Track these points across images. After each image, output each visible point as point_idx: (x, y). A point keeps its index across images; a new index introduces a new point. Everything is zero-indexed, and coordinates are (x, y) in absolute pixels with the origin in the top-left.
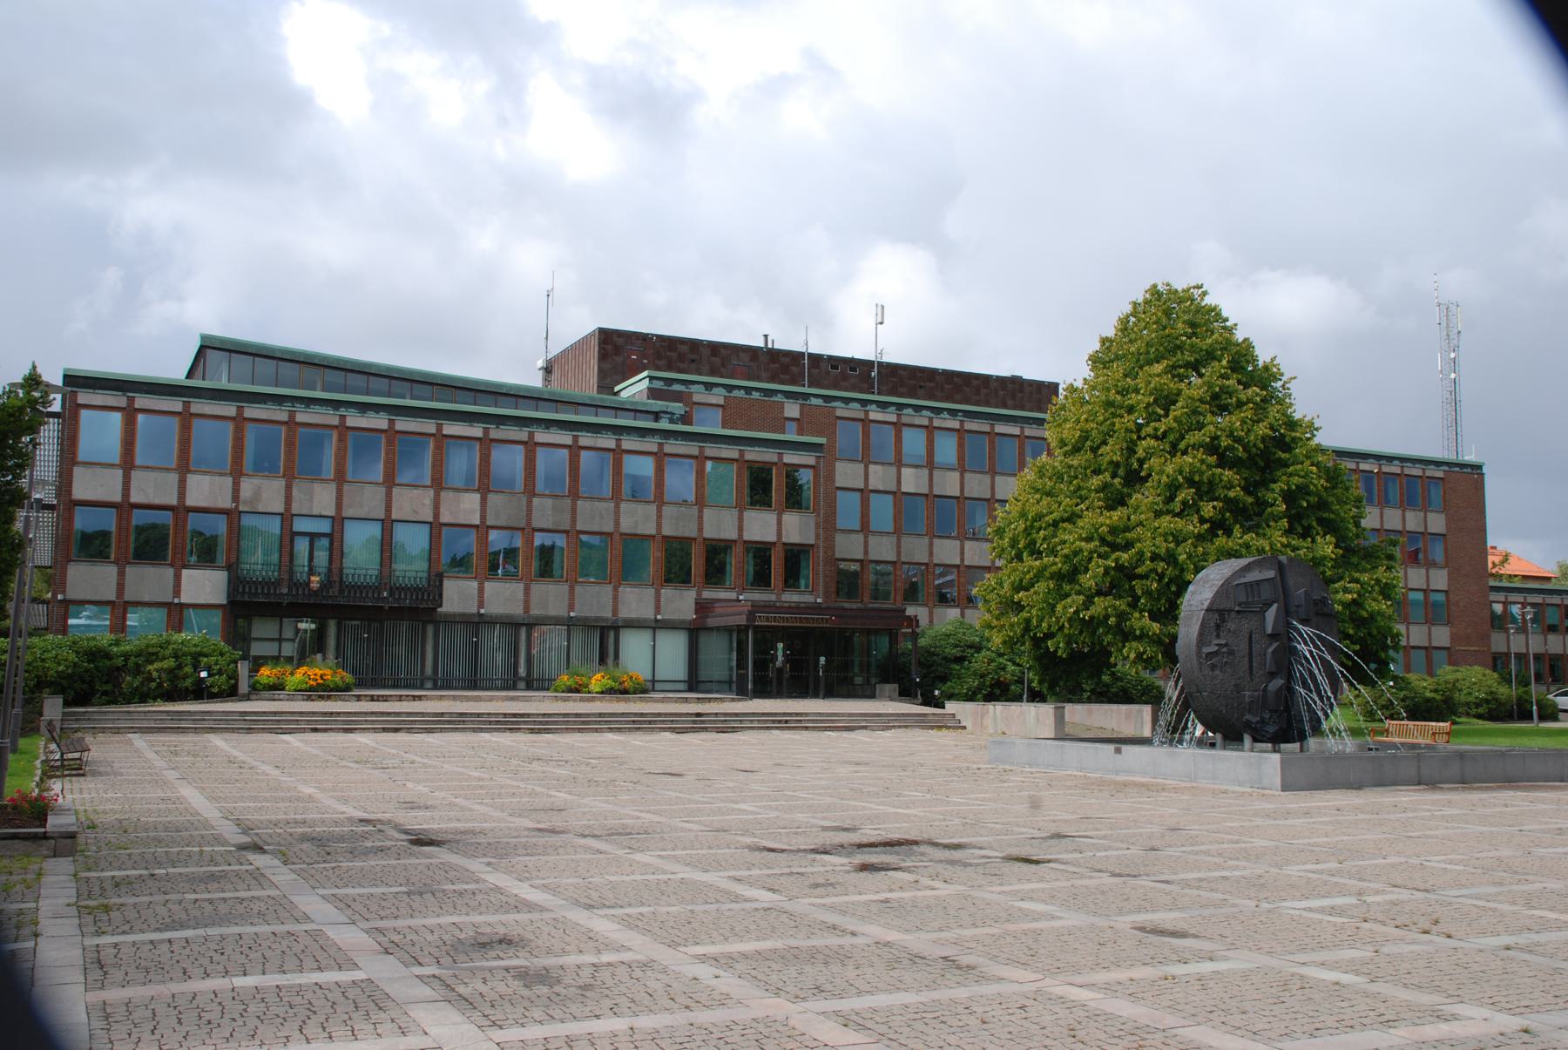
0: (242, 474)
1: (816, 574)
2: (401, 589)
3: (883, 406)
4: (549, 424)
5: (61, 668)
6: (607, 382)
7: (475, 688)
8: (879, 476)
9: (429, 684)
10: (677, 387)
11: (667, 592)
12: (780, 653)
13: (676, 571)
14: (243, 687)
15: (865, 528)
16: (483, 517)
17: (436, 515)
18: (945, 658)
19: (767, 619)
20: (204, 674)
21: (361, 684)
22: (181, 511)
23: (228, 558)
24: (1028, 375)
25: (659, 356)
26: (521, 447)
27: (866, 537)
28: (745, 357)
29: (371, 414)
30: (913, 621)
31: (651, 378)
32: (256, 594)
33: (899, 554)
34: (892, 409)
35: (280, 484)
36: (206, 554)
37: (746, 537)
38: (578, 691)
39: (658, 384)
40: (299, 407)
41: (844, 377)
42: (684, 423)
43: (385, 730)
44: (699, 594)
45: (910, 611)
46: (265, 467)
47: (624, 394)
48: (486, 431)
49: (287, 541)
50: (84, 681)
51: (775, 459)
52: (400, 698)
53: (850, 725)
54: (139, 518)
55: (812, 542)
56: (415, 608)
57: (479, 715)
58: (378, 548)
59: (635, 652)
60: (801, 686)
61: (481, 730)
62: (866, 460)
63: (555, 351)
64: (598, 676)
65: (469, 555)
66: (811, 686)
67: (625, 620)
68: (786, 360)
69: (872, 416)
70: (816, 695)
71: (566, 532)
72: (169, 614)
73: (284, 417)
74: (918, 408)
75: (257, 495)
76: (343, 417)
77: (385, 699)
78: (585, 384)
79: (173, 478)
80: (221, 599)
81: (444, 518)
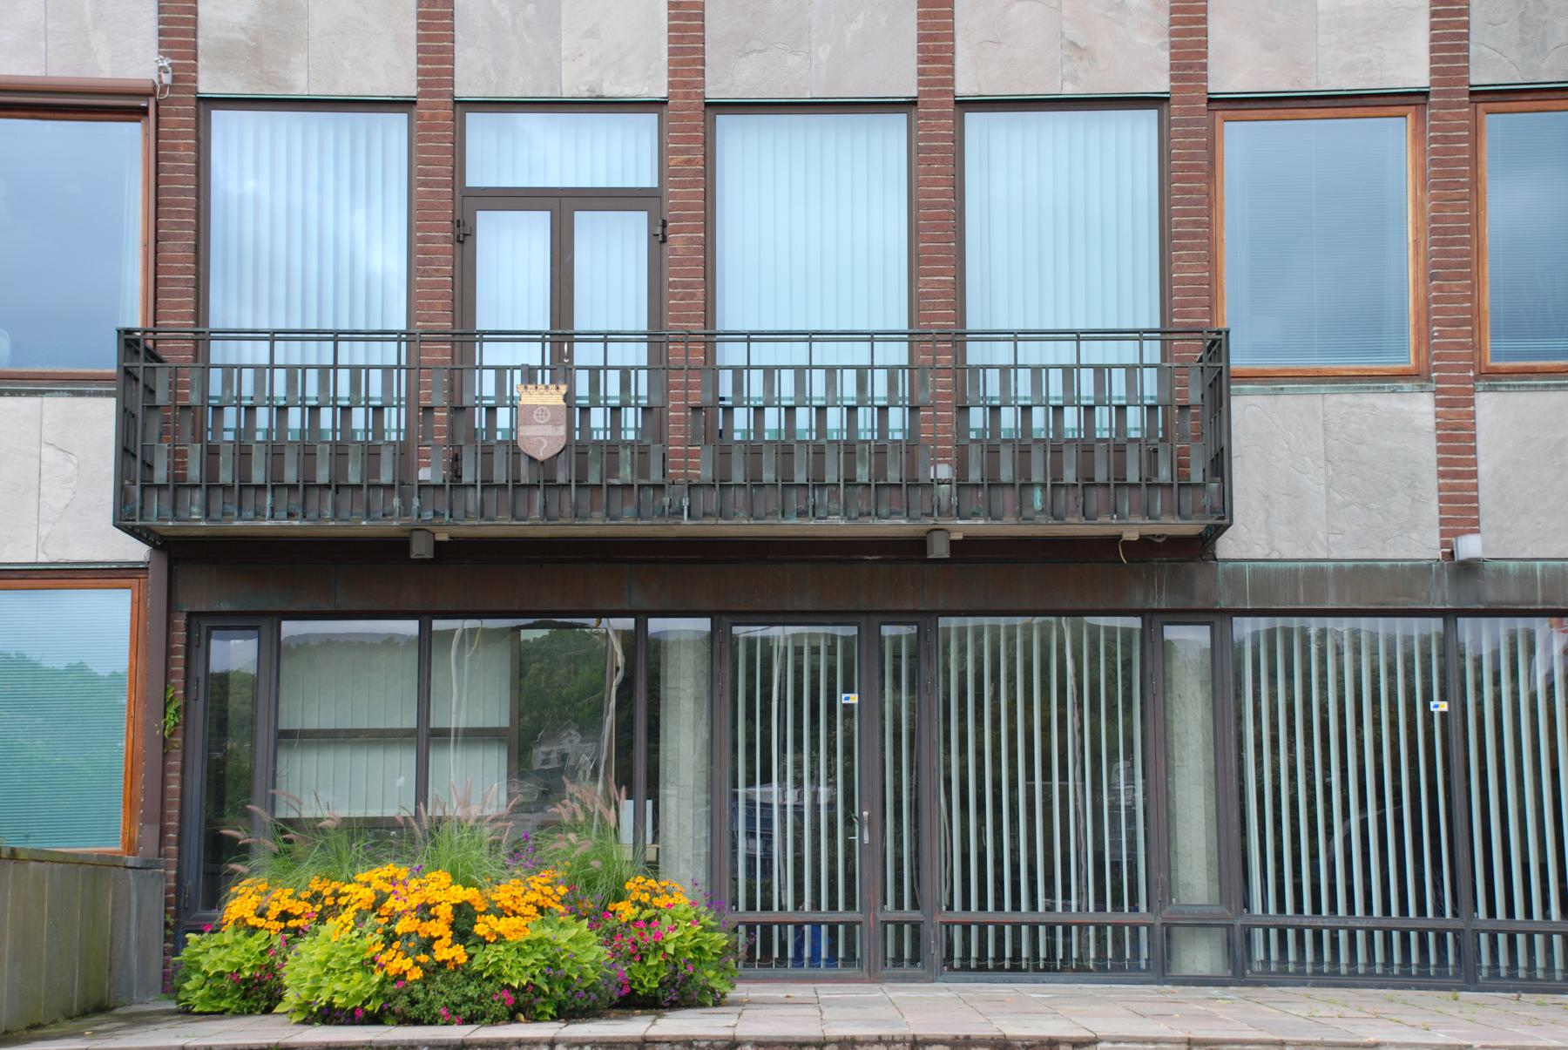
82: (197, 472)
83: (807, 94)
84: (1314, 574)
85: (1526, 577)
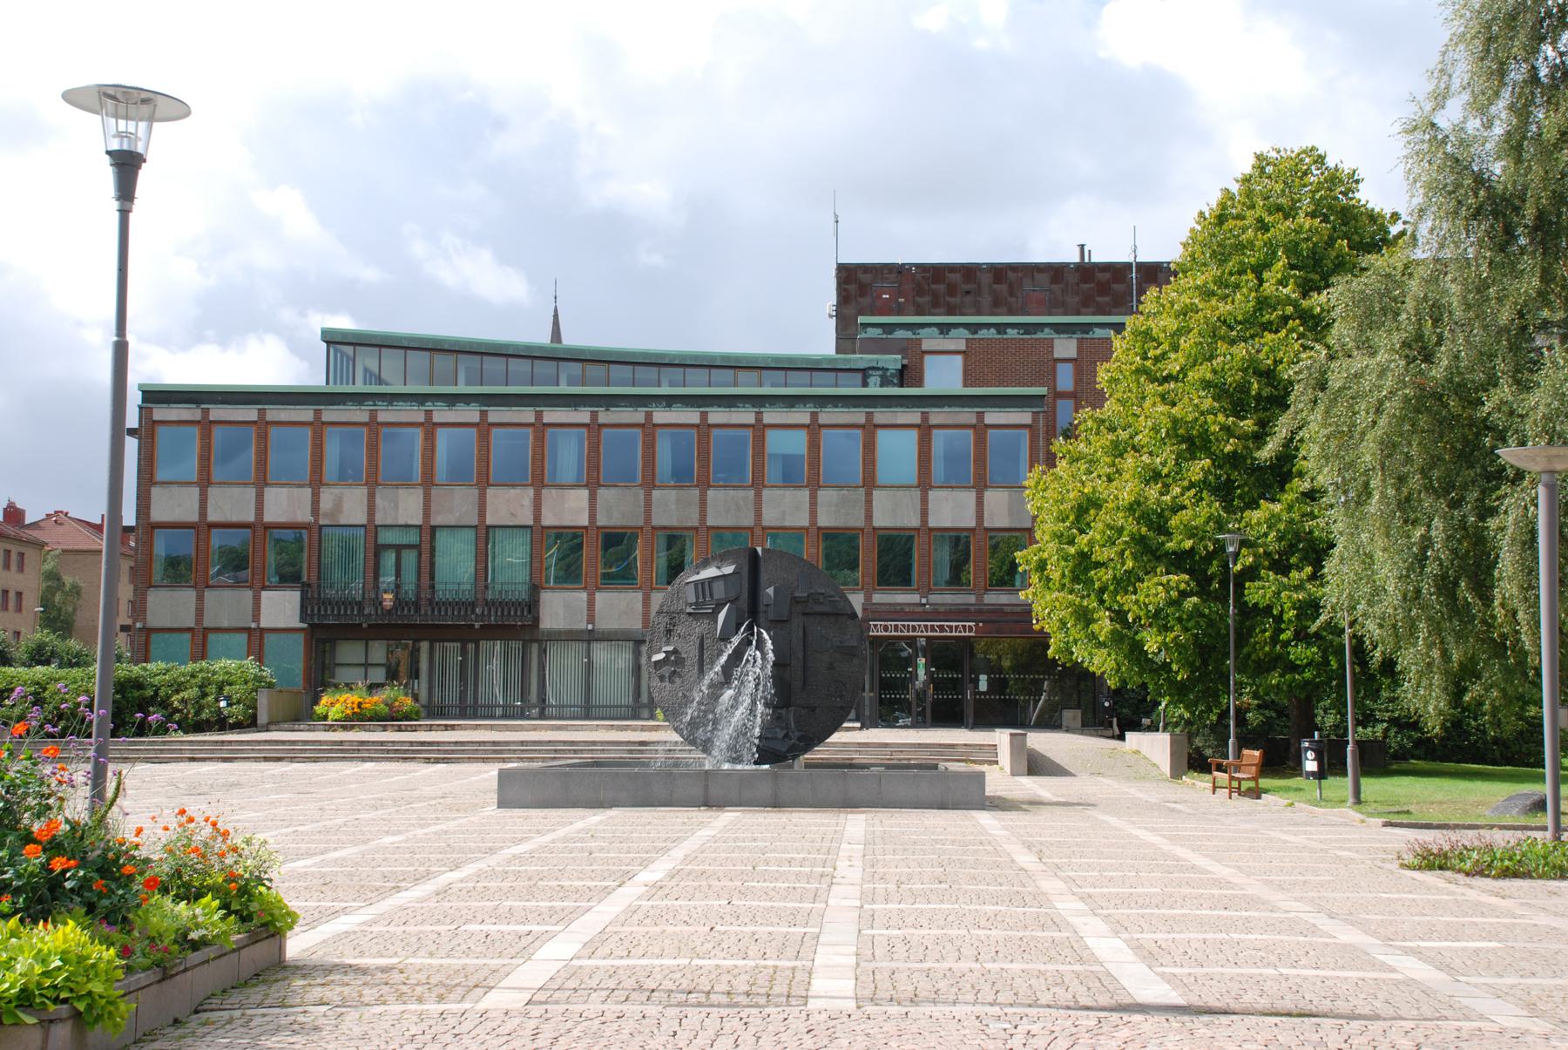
0: (210, 483)
2: (503, 604)
3: (944, 329)
4: (670, 401)
9: (645, 713)
12: (921, 672)
14: (262, 718)
24: (1101, 254)
25: (920, 291)
28: (1044, 279)
32: (326, 616)
35: (362, 492)
36: (288, 578)
37: (932, 523)
44: (868, 598)
46: (345, 478)
48: (594, 415)
49: (371, 555)
73: (365, 417)
76: (429, 413)
79: (251, 492)
84: (560, 632)
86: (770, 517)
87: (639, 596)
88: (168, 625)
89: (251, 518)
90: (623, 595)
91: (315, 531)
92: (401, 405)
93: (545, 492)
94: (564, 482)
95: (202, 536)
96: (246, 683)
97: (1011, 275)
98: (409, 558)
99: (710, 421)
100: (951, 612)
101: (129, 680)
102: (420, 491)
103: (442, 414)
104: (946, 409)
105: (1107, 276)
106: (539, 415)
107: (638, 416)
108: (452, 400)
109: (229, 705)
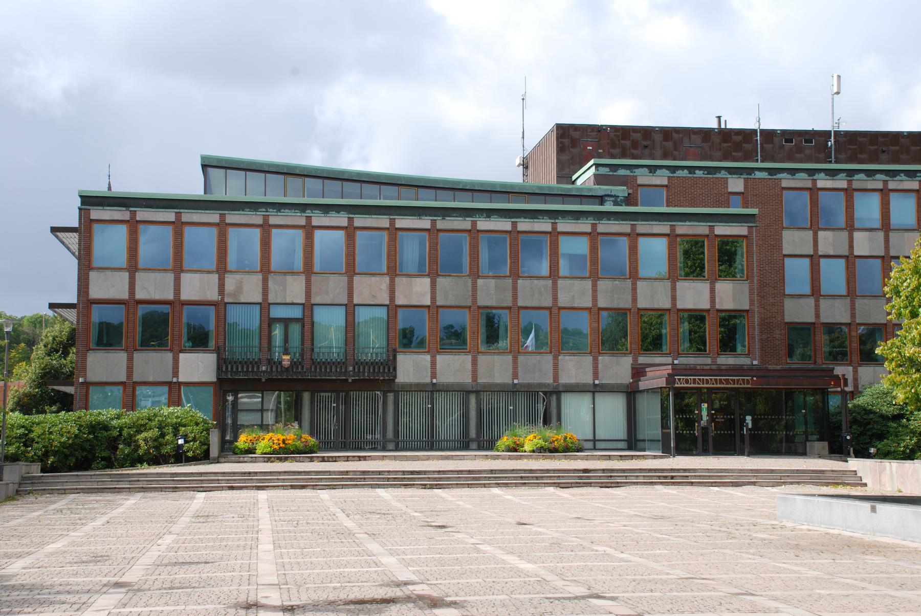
1: (752, 338)
3: (832, 173)
4: (489, 213)
5: (64, 439)
6: (566, 170)
7: (432, 449)
8: (828, 241)
9: (391, 446)
10: (622, 172)
11: (604, 360)
12: (704, 413)
13: (611, 341)
14: (214, 451)
15: (816, 291)
16: (433, 298)
17: (392, 298)
18: (882, 416)
19: (727, 381)
20: (181, 442)
21: (326, 445)
22: (177, 303)
23: (217, 343)
24: (734, 123)
25: (613, 145)
26: (625, 239)
27: (817, 301)
28: (697, 139)
29: (333, 214)
30: (839, 381)
31: (597, 165)
32: (237, 372)
33: (853, 315)
34: (843, 175)
36: (199, 340)
37: (680, 306)
38: (516, 451)
39: (604, 171)
40: (272, 212)
41: (799, 149)
42: (627, 205)
43: (293, 487)
44: (635, 359)
45: (839, 370)
47: (579, 182)
48: (434, 223)
49: (265, 326)
50: (83, 449)
51: (706, 231)
52: (347, 459)
53: (738, 480)
54: (97, 314)
55: (747, 307)
56: (378, 378)
57: (380, 473)
58: (344, 330)
59: (577, 414)
60: (724, 445)
61: (379, 486)
62: (815, 227)
63: (529, 147)
64: (531, 437)
65: (122, 323)
66: (738, 442)
67: (565, 385)
68: (739, 138)
69: (820, 184)
70: (742, 453)
71: (509, 308)
72: (170, 389)
74: (870, 173)
75: (239, 289)
76: (309, 218)
77: (335, 460)
78: (547, 177)
79: (170, 277)
80: (212, 377)
81: (400, 301)
82: (625, 226)
83: (329, 303)
84: (411, 385)
85: (443, 385)
86: (187, 294)
87: (469, 358)
88: (105, 380)
89: (171, 297)
90: (457, 357)
91: (221, 306)
92: (287, 212)
93: (397, 279)
94: (409, 273)
95: (131, 310)
96: (197, 424)
97: (675, 136)
98: (295, 329)
99: (519, 229)
100: (729, 370)
101: (99, 423)
102: (302, 278)
103: (318, 219)
104: (687, 223)
105: (740, 138)
106: (392, 222)
107: (466, 224)
108: (326, 209)
109: (186, 442)
